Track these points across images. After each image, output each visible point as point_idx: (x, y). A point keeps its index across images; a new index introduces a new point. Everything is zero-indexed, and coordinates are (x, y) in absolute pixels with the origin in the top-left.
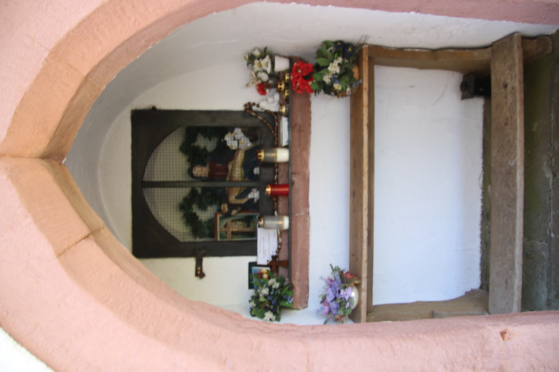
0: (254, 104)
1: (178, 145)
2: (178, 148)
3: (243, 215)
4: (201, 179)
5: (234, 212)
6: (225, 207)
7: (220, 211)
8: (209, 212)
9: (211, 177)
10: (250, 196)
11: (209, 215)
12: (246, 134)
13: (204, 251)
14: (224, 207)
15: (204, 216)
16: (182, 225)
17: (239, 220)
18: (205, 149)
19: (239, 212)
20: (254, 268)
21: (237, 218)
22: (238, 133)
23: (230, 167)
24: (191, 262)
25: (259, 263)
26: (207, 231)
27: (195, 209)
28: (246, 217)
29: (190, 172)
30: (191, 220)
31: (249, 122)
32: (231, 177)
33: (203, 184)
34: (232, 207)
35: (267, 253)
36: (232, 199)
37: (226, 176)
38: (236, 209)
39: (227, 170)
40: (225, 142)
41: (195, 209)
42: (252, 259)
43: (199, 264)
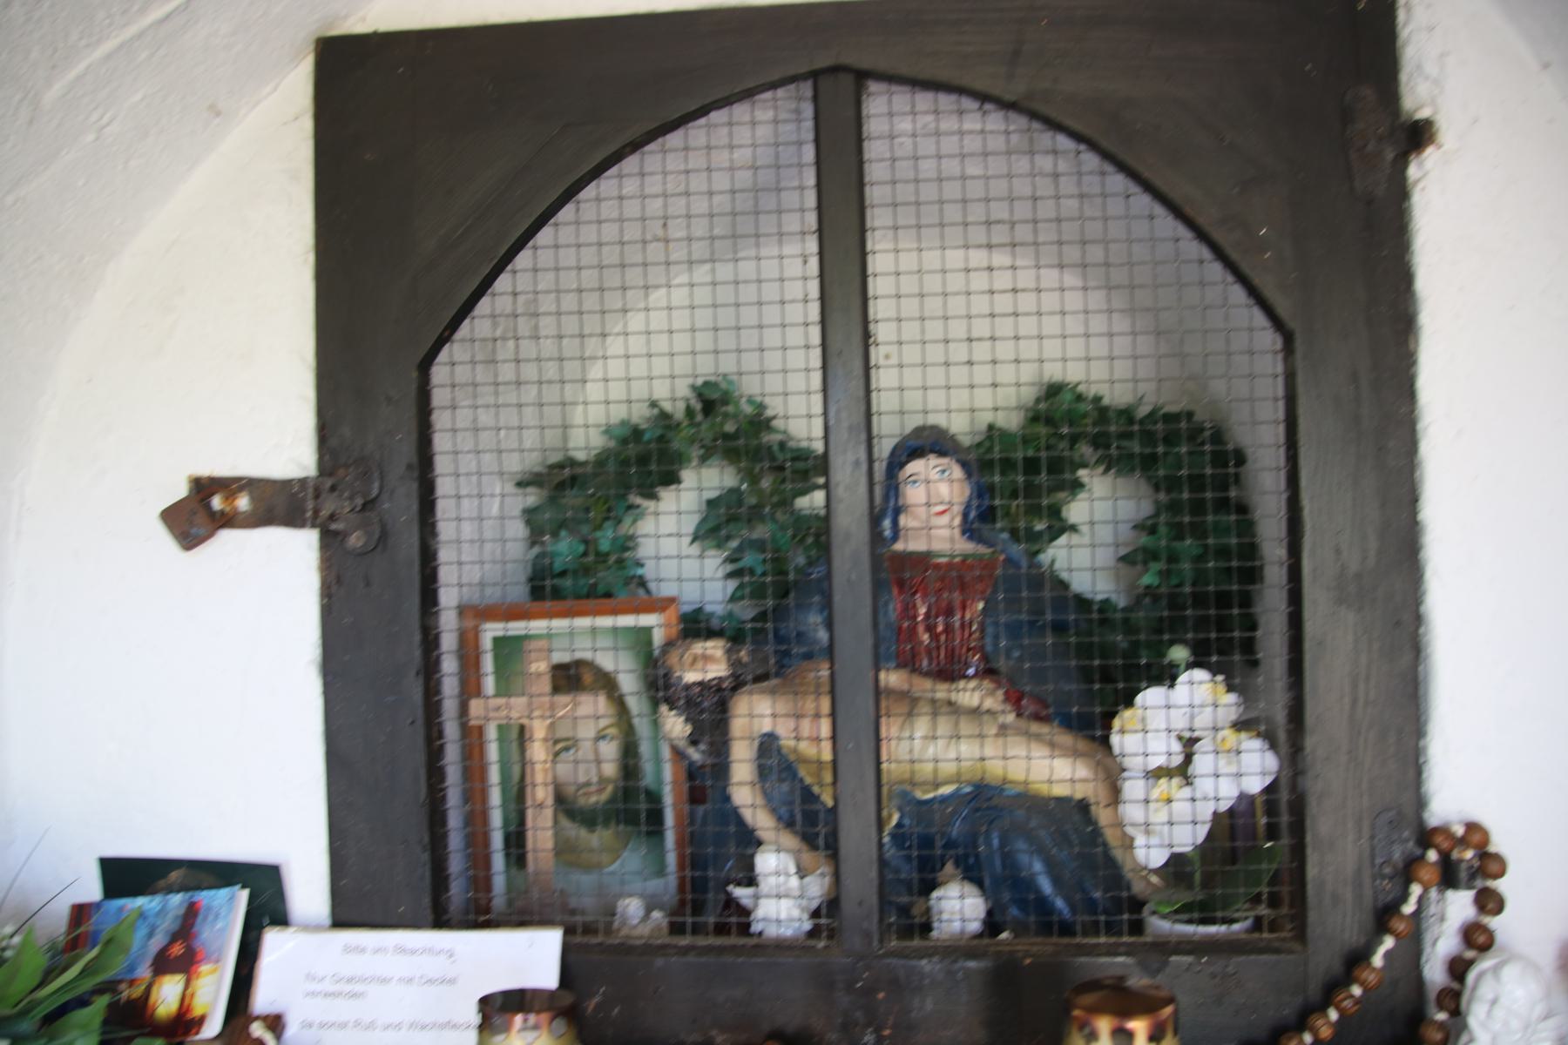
0: (1490, 902)
1: (1099, 371)
2: (1073, 373)
3: (666, 780)
4: (886, 504)
5: (676, 725)
6: (707, 663)
7: (695, 626)
8: (691, 567)
9: (899, 572)
10: (774, 863)
11: (669, 569)
12: (1233, 832)
13: (355, 540)
14: (707, 658)
15: (671, 540)
16: (618, 413)
17: (629, 751)
18: (1060, 527)
19: (678, 753)
20: (229, 908)
21: (645, 749)
22: (1245, 769)
23: (970, 694)
24: (286, 446)
25: (274, 942)
26: (565, 548)
27: (702, 482)
28: (654, 798)
29: (927, 442)
30: (643, 458)
31: (1338, 859)
32: (910, 703)
33: (850, 524)
34: (710, 711)
35: (343, 1010)
36: (756, 715)
37: (908, 662)
38: (693, 741)
39: (949, 673)
40: (1167, 676)
41: (702, 482)
42: (309, 889)
43: (278, 504)
